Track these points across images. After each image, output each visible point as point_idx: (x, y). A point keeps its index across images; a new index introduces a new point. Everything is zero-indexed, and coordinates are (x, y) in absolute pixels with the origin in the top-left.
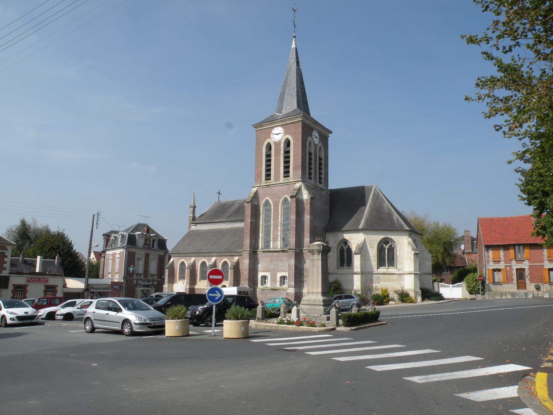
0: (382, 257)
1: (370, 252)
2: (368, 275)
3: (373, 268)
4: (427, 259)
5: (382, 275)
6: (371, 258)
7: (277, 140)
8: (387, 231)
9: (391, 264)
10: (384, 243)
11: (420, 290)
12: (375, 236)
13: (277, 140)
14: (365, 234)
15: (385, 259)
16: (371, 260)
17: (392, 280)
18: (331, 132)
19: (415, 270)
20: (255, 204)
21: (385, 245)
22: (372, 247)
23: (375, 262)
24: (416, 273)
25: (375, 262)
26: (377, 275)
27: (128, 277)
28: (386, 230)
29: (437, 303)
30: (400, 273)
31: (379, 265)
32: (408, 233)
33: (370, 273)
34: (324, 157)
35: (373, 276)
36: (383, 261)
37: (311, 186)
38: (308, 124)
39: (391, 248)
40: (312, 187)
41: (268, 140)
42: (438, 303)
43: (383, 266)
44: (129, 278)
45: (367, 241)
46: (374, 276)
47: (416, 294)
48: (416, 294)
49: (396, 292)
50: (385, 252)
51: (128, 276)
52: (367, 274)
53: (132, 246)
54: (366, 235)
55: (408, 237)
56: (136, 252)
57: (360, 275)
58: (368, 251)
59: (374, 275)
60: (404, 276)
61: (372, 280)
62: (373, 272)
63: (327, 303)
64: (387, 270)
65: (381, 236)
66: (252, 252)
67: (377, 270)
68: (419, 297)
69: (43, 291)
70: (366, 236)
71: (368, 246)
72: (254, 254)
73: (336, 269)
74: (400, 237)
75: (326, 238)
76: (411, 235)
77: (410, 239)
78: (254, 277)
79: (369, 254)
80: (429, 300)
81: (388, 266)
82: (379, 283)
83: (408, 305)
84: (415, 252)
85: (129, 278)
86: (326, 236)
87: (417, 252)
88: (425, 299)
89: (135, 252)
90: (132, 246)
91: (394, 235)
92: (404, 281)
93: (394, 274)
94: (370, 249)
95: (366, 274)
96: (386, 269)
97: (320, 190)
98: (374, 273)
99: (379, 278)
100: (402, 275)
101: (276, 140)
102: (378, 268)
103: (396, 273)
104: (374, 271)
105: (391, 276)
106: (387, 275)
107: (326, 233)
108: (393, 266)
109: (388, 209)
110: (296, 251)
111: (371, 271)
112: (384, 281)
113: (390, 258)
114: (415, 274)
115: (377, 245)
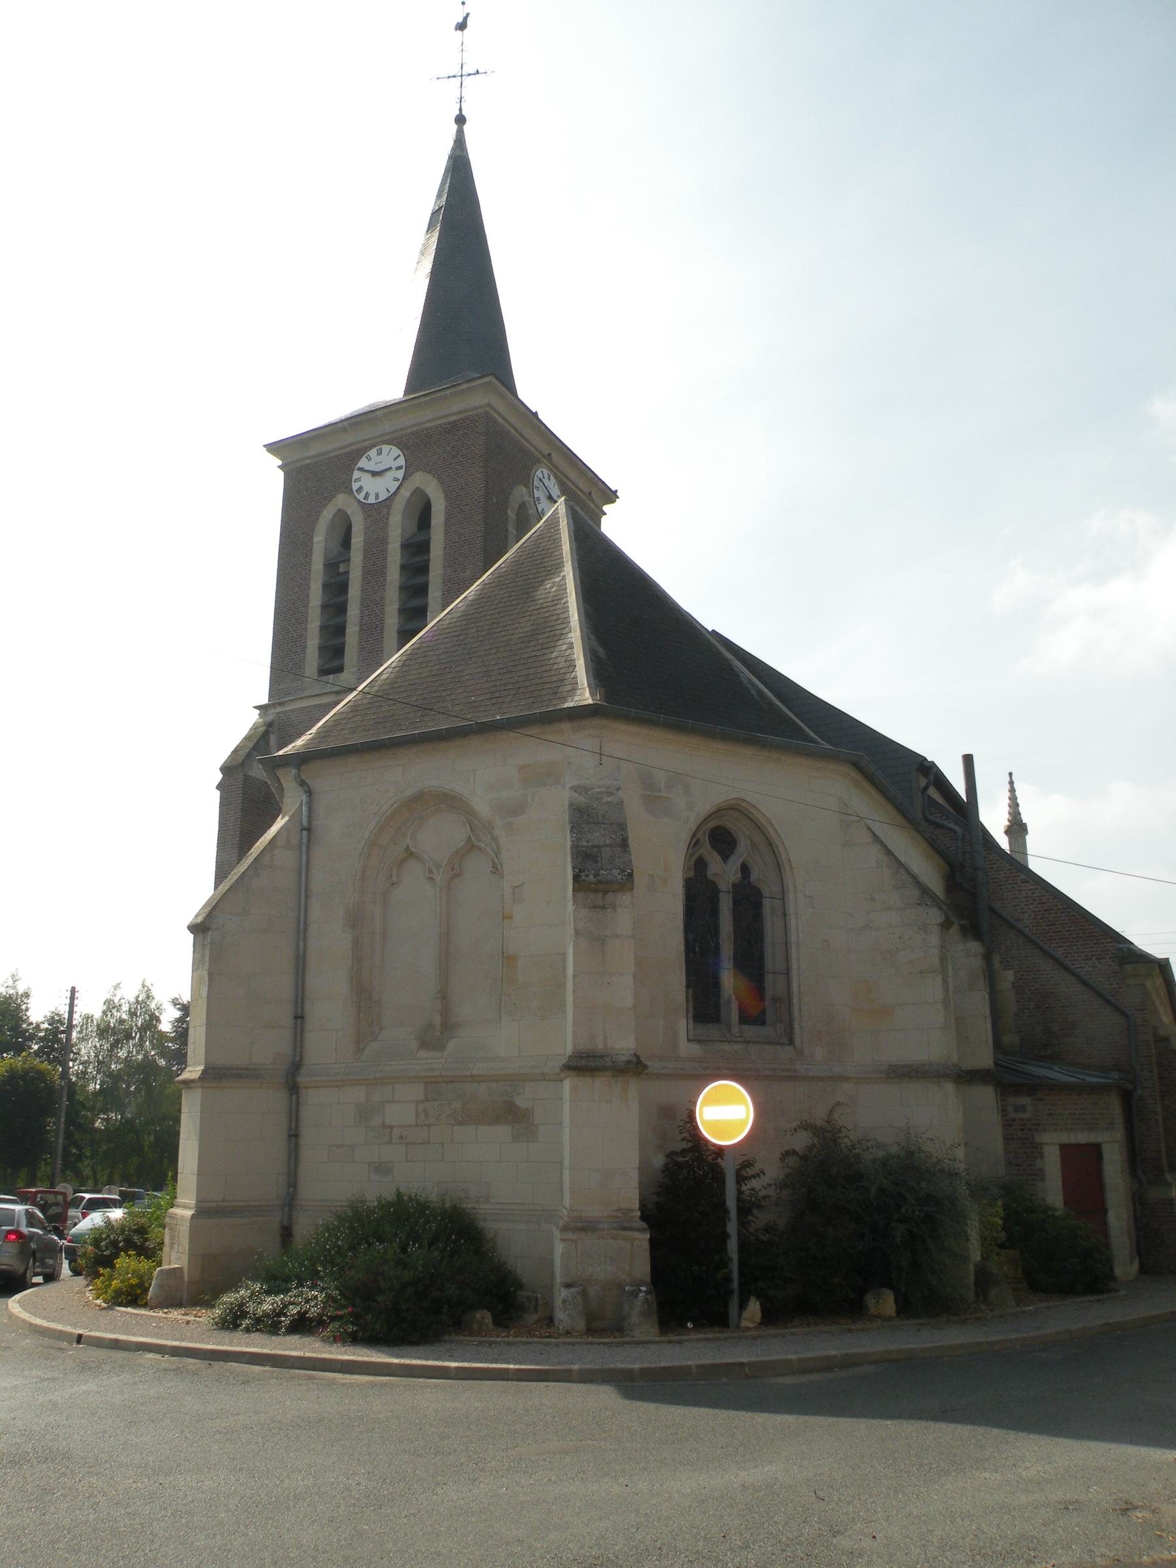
7: (377, 496)
13: (377, 496)
38: (322, 454)
41: (341, 501)
101: (372, 500)
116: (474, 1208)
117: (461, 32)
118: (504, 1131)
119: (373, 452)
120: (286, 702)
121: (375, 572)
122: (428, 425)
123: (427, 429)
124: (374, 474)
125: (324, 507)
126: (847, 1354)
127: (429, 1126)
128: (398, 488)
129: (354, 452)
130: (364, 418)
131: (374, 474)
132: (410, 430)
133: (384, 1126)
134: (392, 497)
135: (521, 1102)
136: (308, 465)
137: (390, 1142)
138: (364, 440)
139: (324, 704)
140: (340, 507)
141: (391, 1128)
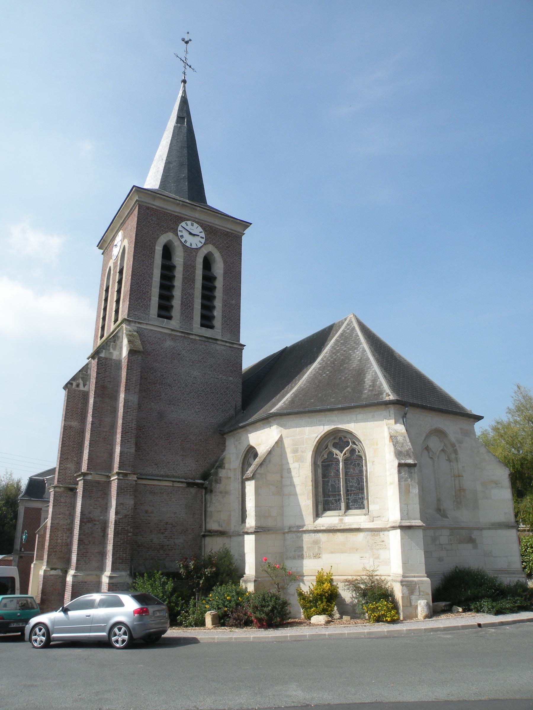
0: (330, 484)
1: (294, 473)
2: (289, 536)
3: (302, 515)
4: (496, 483)
5: (325, 534)
6: (298, 489)
8: (336, 412)
9: (355, 501)
10: (335, 446)
11: (428, 579)
12: (307, 429)
14: (281, 426)
15: (339, 488)
16: (297, 495)
17: (355, 549)
18: (246, 225)
19: (405, 513)
20: (80, 391)
21: (336, 451)
22: (299, 460)
23: (308, 499)
24: (406, 523)
25: (308, 499)
26: (313, 535)
27: (23, 550)
28: (331, 410)
29: (472, 627)
30: (375, 527)
31: (324, 507)
32: (392, 409)
33: (295, 529)
34: (225, 273)
35: (302, 536)
36: (334, 496)
37: (166, 334)
38: (163, 208)
39: (355, 456)
40: (170, 335)
42: (479, 625)
43: (335, 510)
44: (25, 552)
45: (287, 442)
46: (307, 539)
47: (412, 592)
48: (412, 592)
49: (354, 585)
50: (338, 471)
51: (23, 549)
52: (288, 533)
53: (32, 499)
54: (285, 429)
55: (392, 421)
56: (43, 509)
57: (254, 536)
58: (289, 471)
59: (304, 535)
60: (388, 536)
61: (301, 548)
62: (303, 526)
63: (401, 605)
64: (341, 520)
65: (322, 427)
66: (62, 489)
67: (312, 519)
68: (419, 601)
69: (14, 577)
70: (285, 432)
71: (290, 456)
72: (70, 493)
73: (240, 523)
74: (372, 423)
75: (227, 448)
76: (407, 416)
77: (400, 428)
78: (67, 545)
79: (291, 478)
80: (464, 611)
81: (348, 508)
82: (317, 556)
83: (346, 631)
84: (403, 462)
85: (25, 552)
86: (224, 444)
87: (410, 461)
88: (455, 607)
89: (41, 509)
90: (32, 499)
91: (356, 421)
92: (389, 549)
93: (358, 530)
94: (293, 465)
95: (284, 533)
96: (337, 518)
97: (205, 341)
98: (304, 529)
99: (316, 542)
100: (381, 533)
102: (317, 515)
103: (363, 526)
104: (306, 523)
105: (351, 536)
106: (339, 535)
107: (225, 436)
108: (360, 508)
109: (360, 361)
110: (89, 477)
111: (298, 523)
112: (332, 553)
113: (352, 486)
114: (402, 528)
115: (311, 453)
116: (23, 610)
117: (186, 44)
118: (470, 546)
119: (189, 223)
120: (143, 323)
121: (189, 280)
122: (217, 226)
123: (215, 228)
124: (190, 234)
125: (162, 234)
126: (410, 630)
127: (451, 544)
128: (201, 247)
129: (178, 216)
130: (150, 192)
131: (190, 234)
132: (208, 224)
133: (440, 544)
134: (198, 249)
135: (473, 537)
136: (153, 208)
137: (442, 550)
138: (186, 215)
139: (164, 332)
140: (171, 239)
141: (442, 545)
